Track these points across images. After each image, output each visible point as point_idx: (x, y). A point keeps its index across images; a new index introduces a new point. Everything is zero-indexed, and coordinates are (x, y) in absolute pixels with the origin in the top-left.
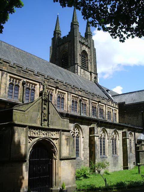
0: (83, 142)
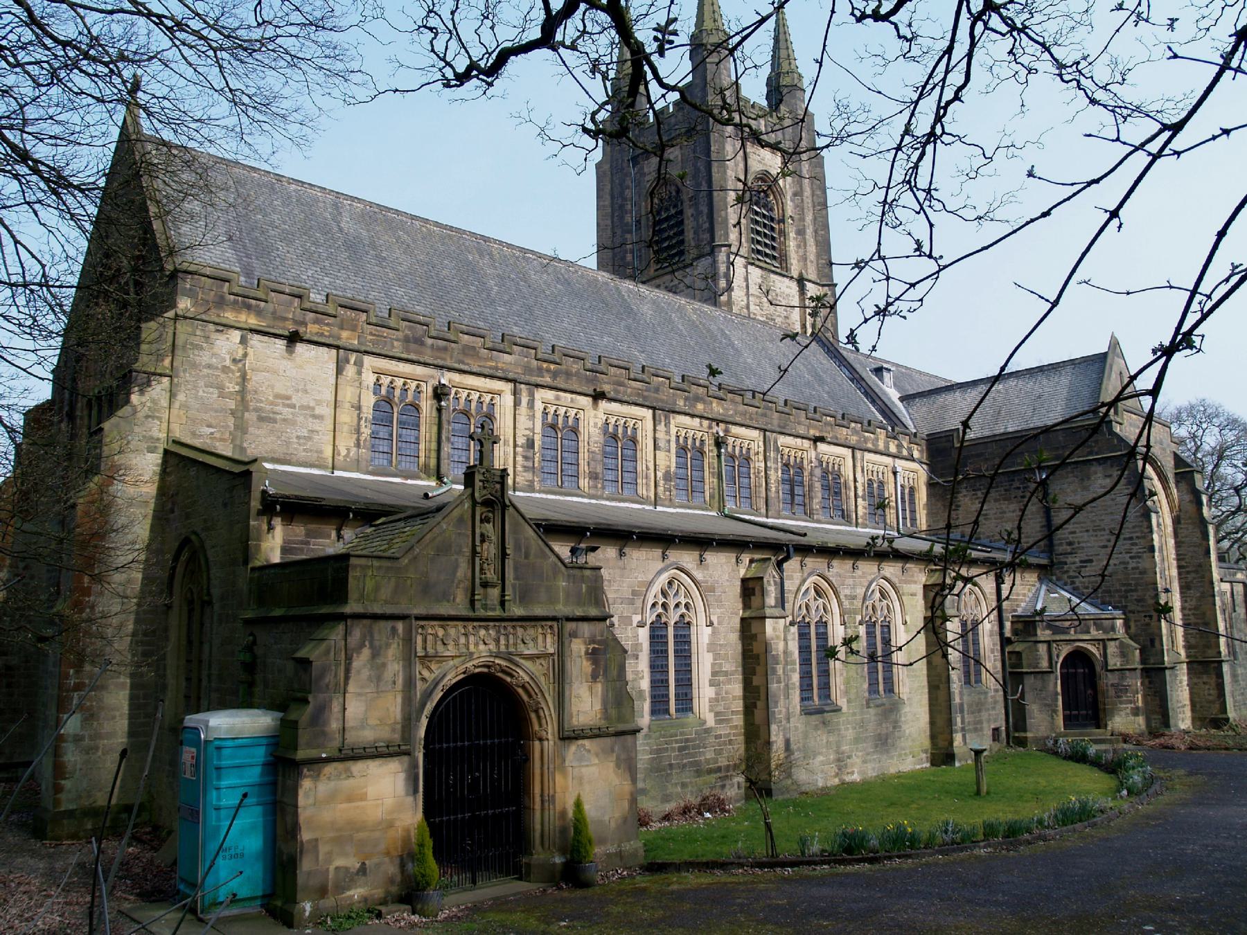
0: (712, 647)
